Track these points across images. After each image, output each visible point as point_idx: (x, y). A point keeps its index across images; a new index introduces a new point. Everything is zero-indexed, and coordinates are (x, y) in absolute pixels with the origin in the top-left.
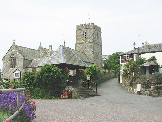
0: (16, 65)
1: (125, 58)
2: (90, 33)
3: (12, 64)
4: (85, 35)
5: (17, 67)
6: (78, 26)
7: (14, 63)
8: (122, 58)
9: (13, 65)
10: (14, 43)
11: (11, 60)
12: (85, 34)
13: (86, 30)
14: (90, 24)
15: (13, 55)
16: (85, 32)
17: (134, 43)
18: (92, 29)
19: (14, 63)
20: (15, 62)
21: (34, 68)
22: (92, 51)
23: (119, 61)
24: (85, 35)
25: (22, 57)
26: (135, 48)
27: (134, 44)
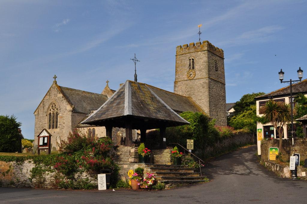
0: (58, 124)
3: (52, 121)
5: (60, 126)
7: (55, 120)
8: (261, 104)
9: (53, 122)
11: (50, 114)
12: (193, 62)
13: (193, 55)
14: (201, 43)
16: (193, 59)
17: (280, 71)
18: (206, 51)
19: (55, 120)
20: (57, 118)
23: (255, 111)
24: (193, 65)
25: (69, 108)
26: (283, 81)
27: (282, 73)
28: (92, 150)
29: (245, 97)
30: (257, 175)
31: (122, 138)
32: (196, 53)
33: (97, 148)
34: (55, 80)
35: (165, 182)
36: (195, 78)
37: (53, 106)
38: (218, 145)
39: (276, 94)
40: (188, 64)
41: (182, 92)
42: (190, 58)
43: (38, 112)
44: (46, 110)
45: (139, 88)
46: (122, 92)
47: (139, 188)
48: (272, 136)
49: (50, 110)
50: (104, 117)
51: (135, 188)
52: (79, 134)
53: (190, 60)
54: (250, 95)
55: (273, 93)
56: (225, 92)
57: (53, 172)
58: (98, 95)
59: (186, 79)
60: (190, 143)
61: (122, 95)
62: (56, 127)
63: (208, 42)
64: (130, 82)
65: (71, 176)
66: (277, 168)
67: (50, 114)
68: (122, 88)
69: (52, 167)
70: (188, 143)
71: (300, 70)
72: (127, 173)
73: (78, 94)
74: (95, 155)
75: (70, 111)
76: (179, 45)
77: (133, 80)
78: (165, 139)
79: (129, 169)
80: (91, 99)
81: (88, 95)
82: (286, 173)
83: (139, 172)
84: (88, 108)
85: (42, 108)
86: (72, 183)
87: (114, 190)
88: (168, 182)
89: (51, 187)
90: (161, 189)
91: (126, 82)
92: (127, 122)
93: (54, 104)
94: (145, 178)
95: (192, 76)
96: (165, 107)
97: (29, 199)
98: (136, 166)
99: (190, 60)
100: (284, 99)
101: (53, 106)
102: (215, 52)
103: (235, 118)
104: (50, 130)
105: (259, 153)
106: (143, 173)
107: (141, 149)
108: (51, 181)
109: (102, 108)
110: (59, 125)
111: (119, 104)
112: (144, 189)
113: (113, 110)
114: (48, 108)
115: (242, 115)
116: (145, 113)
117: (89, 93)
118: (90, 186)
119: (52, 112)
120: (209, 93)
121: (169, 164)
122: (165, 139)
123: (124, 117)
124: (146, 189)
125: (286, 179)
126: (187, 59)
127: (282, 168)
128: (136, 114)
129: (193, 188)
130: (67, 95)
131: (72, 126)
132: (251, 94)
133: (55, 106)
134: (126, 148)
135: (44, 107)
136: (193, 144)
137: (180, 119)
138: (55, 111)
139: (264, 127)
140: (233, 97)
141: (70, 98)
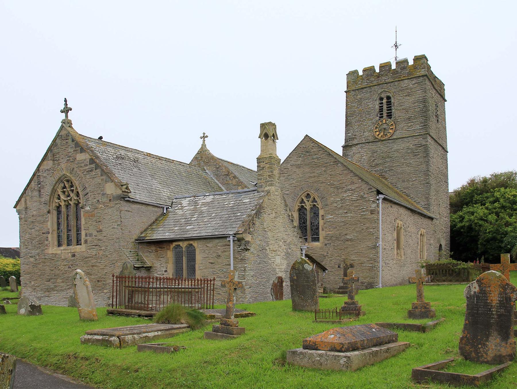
0: (83, 233)
3: (63, 227)
4: (386, 109)
5: (89, 239)
6: (352, 75)
7: (73, 223)
10: (67, 124)
11: (59, 207)
12: (389, 103)
15: (66, 184)
21: (184, 245)
24: (389, 108)
31: (374, 283)
32: (396, 83)
34: (67, 116)
36: (395, 137)
37: (65, 187)
42: (383, 95)
43: (25, 202)
44: (45, 198)
49: (59, 198)
62: (78, 243)
67: (59, 207)
85: (36, 193)
93: (68, 181)
99: (381, 99)
101: (65, 187)
104: (62, 248)
110: (86, 235)
114: (52, 191)
119: (63, 204)
126: (376, 97)
133: (72, 186)
135: (40, 191)
138: (71, 200)
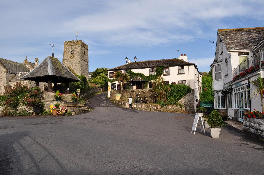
1: (113, 73)
2: (182, 59)
8: (110, 73)
14: (77, 41)
16: (73, 49)
18: (80, 45)
22: (80, 67)
24: (73, 51)
25: (4, 70)
27: (127, 58)
28: (29, 94)
29: (97, 70)
30: (113, 107)
33: (32, 93)
35: (72, 111)
38: (88, 92)
39: (120, 68)
40: (71, 51)
41: (67, 65)
45: (55, 61)
46: (46, 62)
47: (58, 114)
48: (115, 88)
50: (35, 76)
51: (55, 114)
52: (21, 85)
53: (72, 49)
54: (100, 69)
55: (116, 68)
56: (88, 67)
57: (3, 106)
58: (21, 64)
59: (69, 58)
60: (79, 91)
61: (46, 64)
63: (81, 41)
64: (50, 57)
65: (15, 108)
66: (122, 103)
68: (45, 60)
69: (2, 103)
70: (77, 91)
71: (135, 58)
72: (49, 106)
73: (9, 63)
74: (30, 97)
75: (5, 72)
76: (66, 41)
77: (51, 56)
78: (68, 89)
79: (50, 104)
80: (17, 66)
81: (15, 64)
82: (127, 106)
83: (57, 106)
84: (16, 71)
86: (16, 112)
87: (42, 116)
88: (74, 111)
89: (3, 115)
90: (70, 115)
91: (48, 57)
92: (46, 79)
94: (60, 109)
95: (72, 57)
96: (69, 72)
97: (5, 121)
98: (55, 103)
100: (184, 67)
102: (84, 46)
103: (92, 80)
105: (109, 96)
106: (59, 107)
107: (57, 93)
108: (2, 112)
109: (33, 70)
111: (44, 69)
112: (60, 115)
113: (41, 72)
115: (96, 78)
116: (60, 74)
117: (15, 62)
118: (27, 114)
120: (81, 66)
121: (71, 101)
122: (68, 89)
123: (49, 76)
124: (62, 115)
125: (127, 109)
126: (70, 49)
127: (124, 103)
128: (55, 74)
129: (87, 114)
130: (3, 63)
131: (6, 80)
132: (100, 68)
134: (48, 93)
136: (80, 91)
137: (77, 79)
139: (112, 84)
140: (92, 69)
141: (5, 65)
